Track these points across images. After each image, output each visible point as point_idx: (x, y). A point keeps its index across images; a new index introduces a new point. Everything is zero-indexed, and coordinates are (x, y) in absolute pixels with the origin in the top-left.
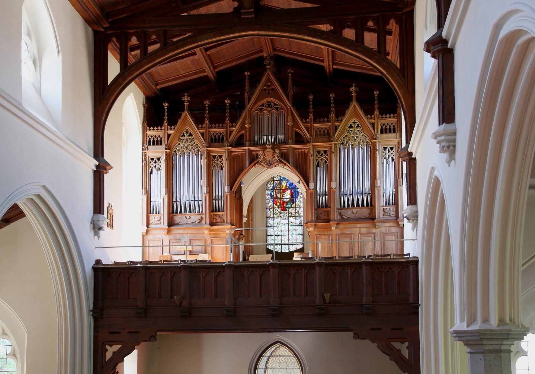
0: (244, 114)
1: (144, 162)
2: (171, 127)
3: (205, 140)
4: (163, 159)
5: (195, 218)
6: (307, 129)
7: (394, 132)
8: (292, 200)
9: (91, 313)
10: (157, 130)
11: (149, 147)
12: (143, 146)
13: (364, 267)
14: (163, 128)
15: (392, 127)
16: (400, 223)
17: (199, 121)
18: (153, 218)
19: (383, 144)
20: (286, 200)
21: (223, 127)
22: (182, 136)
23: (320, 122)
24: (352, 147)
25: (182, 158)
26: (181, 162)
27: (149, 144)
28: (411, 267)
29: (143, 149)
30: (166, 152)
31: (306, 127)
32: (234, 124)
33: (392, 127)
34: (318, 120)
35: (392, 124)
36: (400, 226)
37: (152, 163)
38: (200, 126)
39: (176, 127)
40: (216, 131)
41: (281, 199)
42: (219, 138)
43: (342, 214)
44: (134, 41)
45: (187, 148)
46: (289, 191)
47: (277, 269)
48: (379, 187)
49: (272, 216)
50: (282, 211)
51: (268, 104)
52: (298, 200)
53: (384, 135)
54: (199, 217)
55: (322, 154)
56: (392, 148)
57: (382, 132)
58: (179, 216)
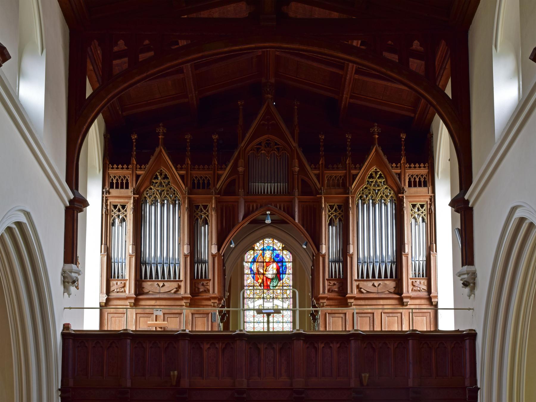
0: (236, 154)
1: (104, 210)
2: (141, 166)
3: (186, 185)
4: (130, 206)
5: (170, 286)
6: (318, 176)
7: (425, 185)
8: (279, 275)
9: (60, 393)
10: (122, 168)
11: (111, 190)
12: (103, 188)
13: (411, 341)
14: (130, 166)
15: (422, 180)
16: (433, 300)
17: (178, 161)
18: (115, 285)
19: (412, 200)
20: (270, 276)
21: (208, 169)
22: (155, 179)
23: (333, 169)
24: (372, 203)
25: (153, 207)
26: (153, 213)
27: (112, 187)
28: (467, 342)
29: (103, 193)
30: (134, 198)
31: (315, 175)
32: (224, 166)
33: (422, 180)
34: (330, 166)
35: (422, 176)
36: (434, 303)
37: (115, 211)
38: (179, 166)
39: (147, 166)
40: (199, 173)
41: (263, 274)
42: (204, 183)
43: (360, 286)
44: (121, 45)
45: (161, 194)
46: (275, 265)
47: (302, 341)
48: (408, 252)
49: (251, 296)
50: (265, 291)
51: (266, 143)
52: (285, 277)
53: (413, 190)
54: (175, 285)
55: (336, 209)
56: (422, 206)
57: (410, 186)
58: (149, 283)
